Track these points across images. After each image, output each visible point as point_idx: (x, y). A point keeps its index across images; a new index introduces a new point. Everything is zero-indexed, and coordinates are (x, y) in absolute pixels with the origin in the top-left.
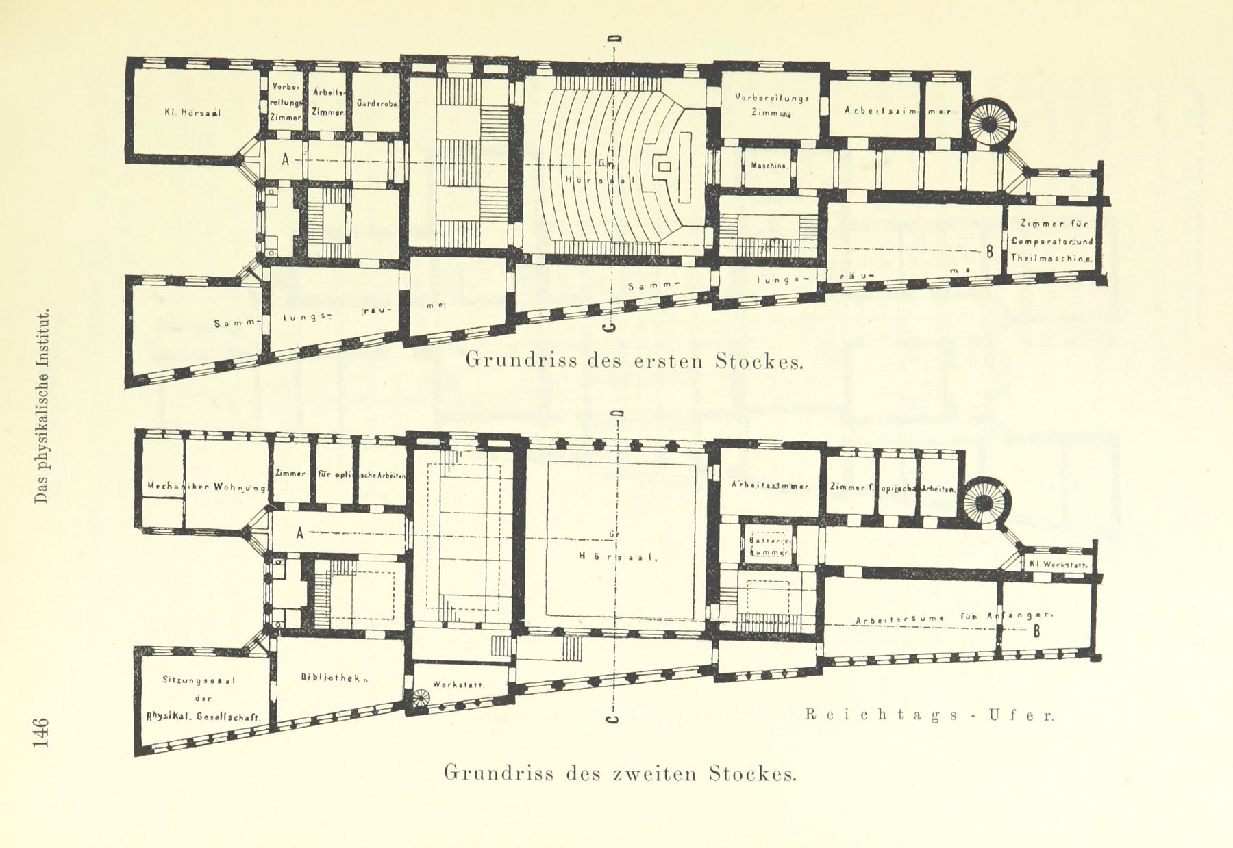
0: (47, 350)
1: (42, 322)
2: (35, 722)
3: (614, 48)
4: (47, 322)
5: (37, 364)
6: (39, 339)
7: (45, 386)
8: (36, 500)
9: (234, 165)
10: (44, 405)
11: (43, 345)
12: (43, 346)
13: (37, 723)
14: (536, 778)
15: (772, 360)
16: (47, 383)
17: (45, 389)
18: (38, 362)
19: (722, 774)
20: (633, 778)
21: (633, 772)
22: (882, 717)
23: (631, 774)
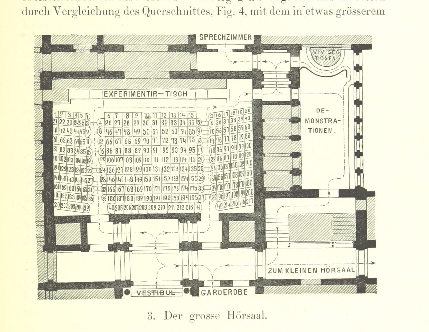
3: (340, 120)
8: (310, 129)
14: (330, 14)
19: (352, 12)
20: (319, 13)
21: (319, 10)
23: (318, 11)
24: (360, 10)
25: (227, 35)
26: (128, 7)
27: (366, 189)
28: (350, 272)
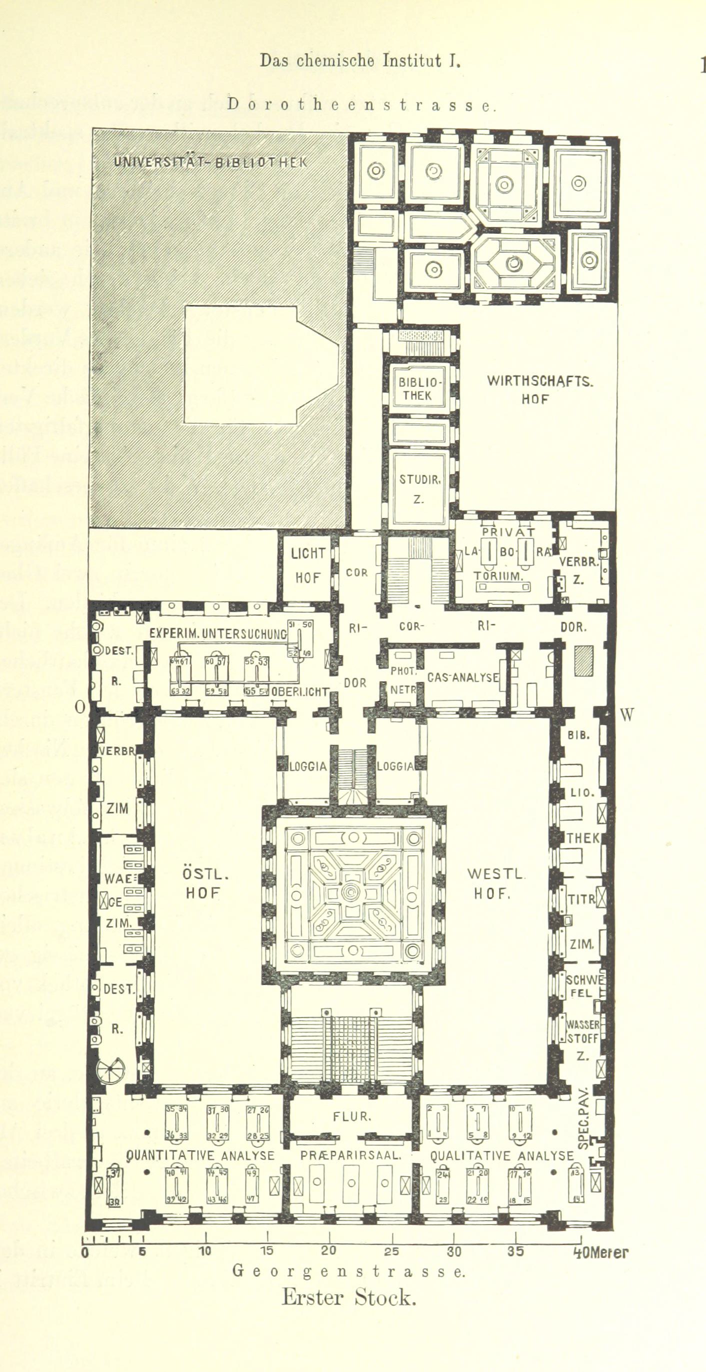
0: (401, 65)
2: (353, 60)
4: (432, 65)
5: (386, 54)
6: (413, 56)
7: (362, 63)
8: (263, 54)
9: (463, 211)
10: (342, 62)
11: (407, 61)
12: (404, 61)
14: (313, 1296)
15: (408, 1296)
17: (358, 64)
18: (388, 56)
19: (368, 1298)
22: (318, 107)
23: (625, 712)
25: (113, 813)
28: (123, 882)
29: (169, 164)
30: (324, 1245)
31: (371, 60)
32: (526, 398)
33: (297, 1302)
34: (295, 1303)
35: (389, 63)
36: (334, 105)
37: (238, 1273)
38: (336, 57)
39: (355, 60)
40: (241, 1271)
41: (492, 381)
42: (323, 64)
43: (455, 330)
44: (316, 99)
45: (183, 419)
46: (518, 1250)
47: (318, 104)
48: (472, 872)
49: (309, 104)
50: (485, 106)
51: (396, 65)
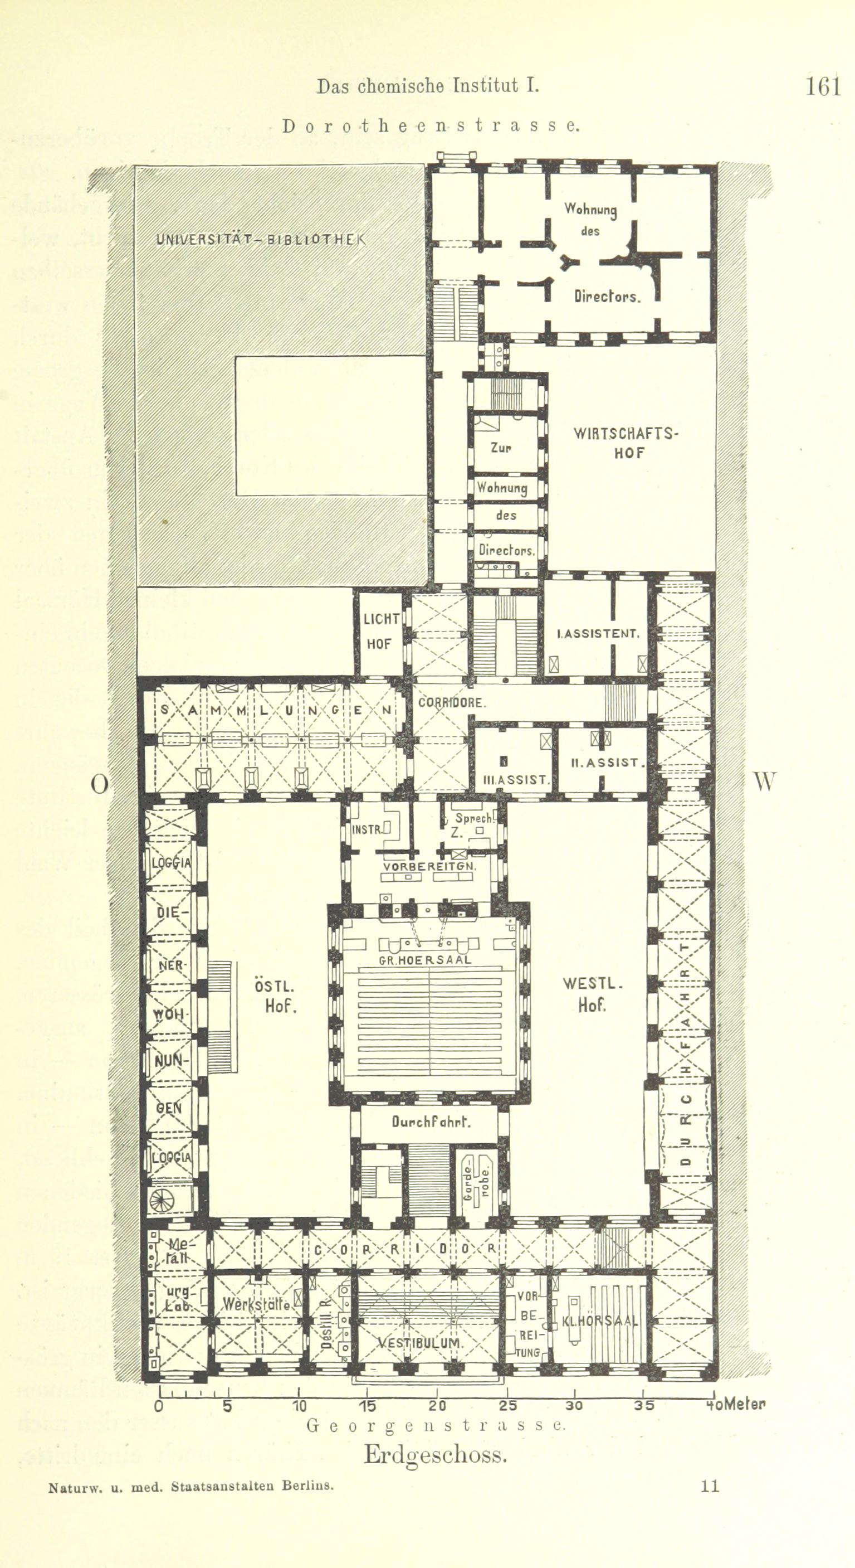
0: (473, 91)
1: (508, 83)
2: (420, 85)
4: (508, 90)
5: (456, 79)
6: (487, 80)
7: (372, 90)
8: (321, 80)
10: (407, 88)
11: (480, 86)
13: (824, 82)
16: (433, 91)
17: (367, 90)
19: (482, 1456)
22: (384, 129)
23: (761, 776)
24: (439, 1453)
26: (402, 1446)
27: (394, 1221)
29: (214, 242)
30: (638, 1400)
31: (440, 85)
32: (618, 453)
33: (381, 1460)
34: (378, 1461)
35: (459, 88)
36: (402, 127)
37: (312, 1428)
38: (401, 82)
39: (364, 85)
40: (316, 1426)
41: (580, 433)
42: (386, 90)
43: (543, 379)
44: (381, 119)
45: (235, 491)
46: (647, 1404)
47: (384, 126)
48: (567, 982)
49: (374, 126)
50: (570, 125)
51: (468, 91)
